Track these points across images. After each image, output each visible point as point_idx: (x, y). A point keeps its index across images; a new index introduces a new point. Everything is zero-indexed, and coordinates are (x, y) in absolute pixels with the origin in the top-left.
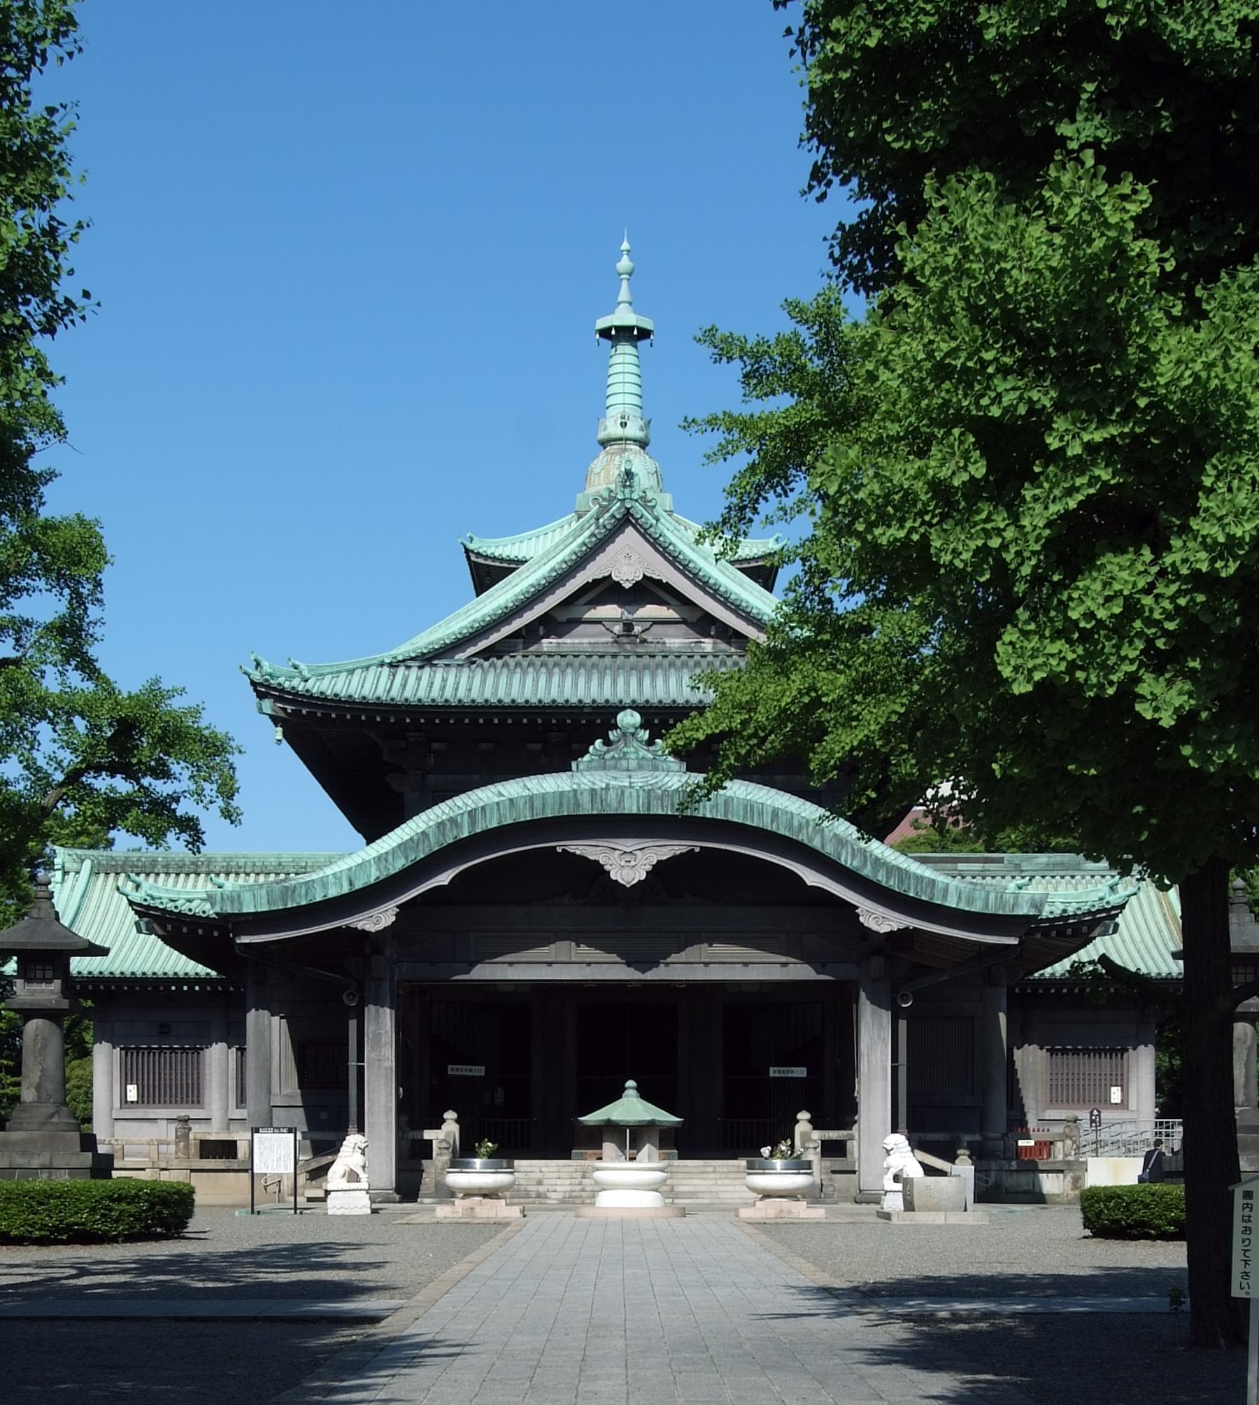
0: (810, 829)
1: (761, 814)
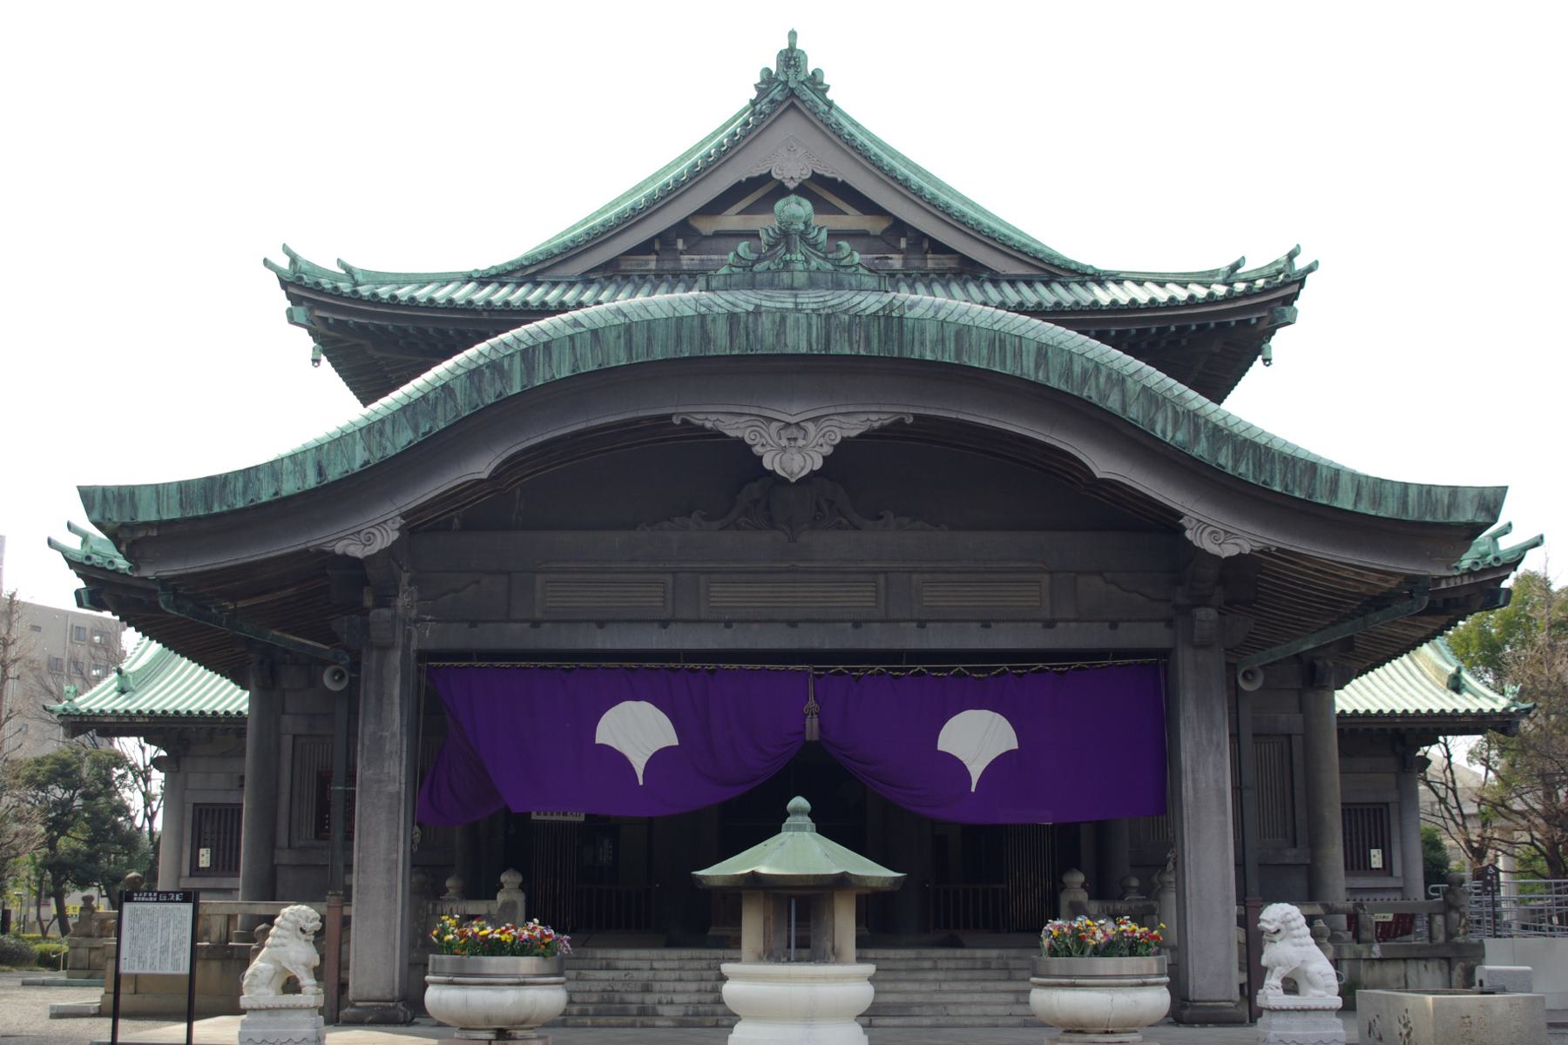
0: (1102, 380)
1: (1018, 354)
